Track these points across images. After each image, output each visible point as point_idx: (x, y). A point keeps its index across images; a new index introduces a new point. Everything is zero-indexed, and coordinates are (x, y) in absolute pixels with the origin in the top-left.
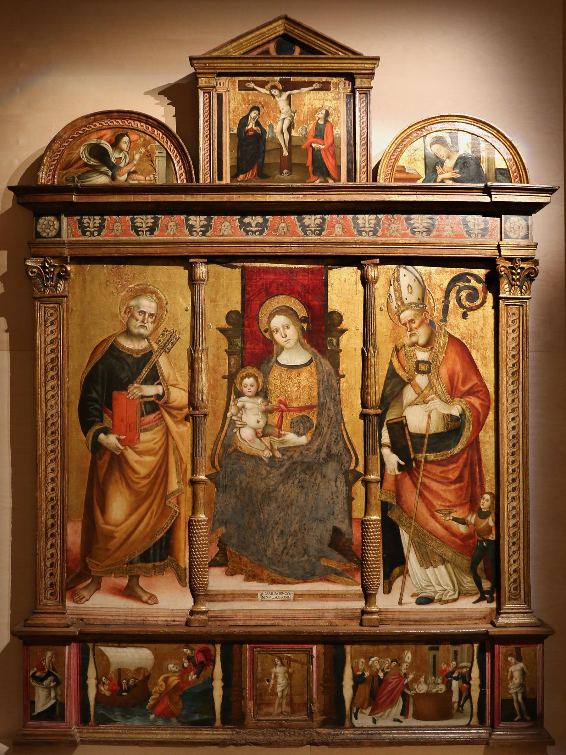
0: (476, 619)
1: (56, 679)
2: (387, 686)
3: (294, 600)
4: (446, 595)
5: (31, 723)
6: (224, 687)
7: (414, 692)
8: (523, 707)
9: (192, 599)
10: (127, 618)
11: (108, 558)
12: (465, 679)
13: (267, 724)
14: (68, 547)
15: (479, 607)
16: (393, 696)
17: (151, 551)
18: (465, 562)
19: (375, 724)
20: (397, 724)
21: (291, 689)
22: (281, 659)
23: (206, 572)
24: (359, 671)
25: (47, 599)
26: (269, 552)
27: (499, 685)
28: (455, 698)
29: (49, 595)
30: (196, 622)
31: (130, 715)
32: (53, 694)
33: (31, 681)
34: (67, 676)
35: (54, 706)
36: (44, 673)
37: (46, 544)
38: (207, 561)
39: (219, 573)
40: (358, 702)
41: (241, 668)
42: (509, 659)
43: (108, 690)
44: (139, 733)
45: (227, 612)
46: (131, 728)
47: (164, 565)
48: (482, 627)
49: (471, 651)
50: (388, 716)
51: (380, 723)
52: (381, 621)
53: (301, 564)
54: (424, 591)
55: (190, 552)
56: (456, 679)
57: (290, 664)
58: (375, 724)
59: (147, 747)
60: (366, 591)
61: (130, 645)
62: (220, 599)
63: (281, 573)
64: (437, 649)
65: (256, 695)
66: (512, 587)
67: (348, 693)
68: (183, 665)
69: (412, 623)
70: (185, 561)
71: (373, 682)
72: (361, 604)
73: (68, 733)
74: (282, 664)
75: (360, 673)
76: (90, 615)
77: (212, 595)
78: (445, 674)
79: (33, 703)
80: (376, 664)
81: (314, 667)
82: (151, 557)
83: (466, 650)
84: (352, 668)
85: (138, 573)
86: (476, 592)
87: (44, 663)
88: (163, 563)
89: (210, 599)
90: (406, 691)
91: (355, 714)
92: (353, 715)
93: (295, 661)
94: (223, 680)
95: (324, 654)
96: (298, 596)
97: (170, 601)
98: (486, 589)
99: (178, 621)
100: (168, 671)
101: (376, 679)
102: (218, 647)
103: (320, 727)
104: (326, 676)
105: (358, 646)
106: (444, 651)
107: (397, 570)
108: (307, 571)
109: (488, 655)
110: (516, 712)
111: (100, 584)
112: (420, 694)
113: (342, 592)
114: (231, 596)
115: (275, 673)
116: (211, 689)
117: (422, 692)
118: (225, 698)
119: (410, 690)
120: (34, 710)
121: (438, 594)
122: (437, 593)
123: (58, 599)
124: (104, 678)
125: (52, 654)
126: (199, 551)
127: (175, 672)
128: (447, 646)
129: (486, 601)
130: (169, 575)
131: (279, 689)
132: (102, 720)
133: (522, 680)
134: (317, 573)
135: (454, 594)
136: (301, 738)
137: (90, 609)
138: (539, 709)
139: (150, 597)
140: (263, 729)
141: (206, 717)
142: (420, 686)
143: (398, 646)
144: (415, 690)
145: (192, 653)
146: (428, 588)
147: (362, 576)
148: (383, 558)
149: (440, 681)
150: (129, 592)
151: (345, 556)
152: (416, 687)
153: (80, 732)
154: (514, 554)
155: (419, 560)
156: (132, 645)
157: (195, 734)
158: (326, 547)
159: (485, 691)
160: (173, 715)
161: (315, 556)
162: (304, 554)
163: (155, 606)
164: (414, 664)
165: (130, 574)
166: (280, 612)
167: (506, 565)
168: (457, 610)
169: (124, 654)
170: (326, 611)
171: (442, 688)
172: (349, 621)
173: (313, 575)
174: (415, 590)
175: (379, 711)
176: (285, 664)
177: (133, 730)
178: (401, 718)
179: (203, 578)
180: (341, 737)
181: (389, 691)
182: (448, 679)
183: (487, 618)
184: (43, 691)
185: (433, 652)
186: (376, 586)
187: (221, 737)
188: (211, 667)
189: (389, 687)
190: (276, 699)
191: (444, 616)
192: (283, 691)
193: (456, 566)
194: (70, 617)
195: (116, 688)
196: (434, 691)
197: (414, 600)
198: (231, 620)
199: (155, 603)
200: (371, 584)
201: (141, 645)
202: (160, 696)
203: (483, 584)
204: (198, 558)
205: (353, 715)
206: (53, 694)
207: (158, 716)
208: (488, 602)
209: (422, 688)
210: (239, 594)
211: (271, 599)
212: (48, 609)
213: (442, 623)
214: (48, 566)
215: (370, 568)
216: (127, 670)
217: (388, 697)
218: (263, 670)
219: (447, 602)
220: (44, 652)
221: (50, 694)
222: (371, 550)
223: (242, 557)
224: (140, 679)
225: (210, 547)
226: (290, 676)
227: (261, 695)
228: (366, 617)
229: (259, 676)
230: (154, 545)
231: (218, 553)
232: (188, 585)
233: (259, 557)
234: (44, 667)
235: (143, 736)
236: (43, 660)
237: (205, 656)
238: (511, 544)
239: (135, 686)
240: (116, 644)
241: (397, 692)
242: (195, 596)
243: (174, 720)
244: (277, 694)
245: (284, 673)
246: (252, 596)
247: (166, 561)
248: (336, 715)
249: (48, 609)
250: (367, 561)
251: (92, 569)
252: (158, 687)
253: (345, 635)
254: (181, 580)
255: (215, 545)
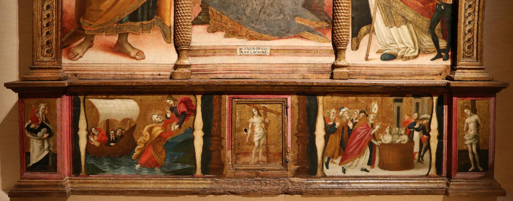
0: (433, 75)
1: (49, 131)
2: (355, 136)
3: (271, 55)
4: (408, 52)
5: (26, 174)
6: (204, 137)
7: (380, 142)
8: (477, 157)
9: (177, 55)
10: (117, 73)
11: (100, 18)
12: (425, 130)
13: (245, 173)
14: (64, 9)
15: (436, 64)
16: (361, 146)
17: (140, 12)
18: (425, 22)
19: (345, 173)
20: (364, 173)
21: (267, 139)
22: (258, 110)
23: (188, 28)
24: (330, 121)
25: (44, 56)
26: (248, 11)
27: (456, 137)
28: (416, 148)
29: (45, 53)
30: (179, 75)
31: (117, 165)
32: (46, 146)
33: (26, 133)
34: (59, 127)
35: (47, 157)
36: (38, 125)
37: (43, 6)
38: (190, 19)
39: (202, 30)
40: (329, 152)
41: (220, 117)
42: (466, 111)
43: (98, 141)
44: (125, 183)
45: (208, 66)
46: (118, 178)
47: (151, 23)
48: (440, 81)
49: (431, 104)
50: (356, 166)
51: (349, 173)
52: (350, 76)
53: (277, 22)
54: (388, 48)
55: (175, 11)
56: (418, 130)
57: (266, 114)
58: (345, 173)
59: (132, 197)
60: (336, 47)
61: (118, 97)
62: (202, 54)
63: (258, 31)
64: (401, 101)
65: (235, 145)
66: (467, 46)
67: (320, 142)
68: (166, 115)
69: (378, 77)
70: (170, 20)
71: (343, 132)
72: (331, 59)
73: (59, 184)
74: (259, 114)
75: (331, 123)
76: (83, 71)
77: (195, 50)
78: (407, 125)
79: (28, 154)
80: (346, 115)
81: (289, 117)
82: (139, 16)
83: (427, 102)
84: (324, 118)
85: (127, 31)
86: (433, 50)
87: (38, 115)
88: (150, 22)
89: (192, 54)
90: (373, 141)
91: (326, 163)
92: (324, 164)
93: (271, 111)
94: (204, 129)
95: (298, 104)
96: (274, 51)
97: (155, 57)
98: (442, 48)
99: (163, 75)
100: (152, 122)
101: (346, 129)
102: (199, 97)
103: (293, 177)
104: (300, 126)
105: (330, 97)
106: (407, 103)
107: (364, 29)
108: (283, 28)
109: (445, 107)
110: (470, 163)
111: (92, 41)
112: (385, 144)
113: (315, 48)
114: (212, 51)
115: (253, 123)
116: (193, 139)
117: (387, 142)
118: (205, 147)
119: (376, 140)
120: (29, 162)
121: (401, 51)
122: (400, 50)
123: (54, 56)
124: (93, 129)
125: (45, 106)
126: (182, 10)
127: (159, 122)
128: (410, 98)
129: (442, 59)
130: (156, 32)
131: (256, 139)
132: (93, 170)
133: (476, 132)
134: (292, 30)
135: (415, 52)
136: (276, 187)
137: (83, 65)
138: (490, 160)
139: (138, 53)
140: (241, 178)
141: (187, 166)
142: (385, 136)
143: (366, 98)
144: (380, 140)
145: (175, 104)
146: (392, 45)
147: (333, 33)
148: (353, 18)
149: (403, 132)
150: (119, 49)
151: (318, 16)
152: (381, 137)
153: (71, 183)
154: (470, 16)
155: (384, 20)
156: (120, 97)
157: (177, 183)
158: (300, 8)
159: (442, 142)
160: (157, 165)
161: (289, 15)
162: (280, 13)
163: (142, 61)
164: (380, 115)
165: (119, 32)
166: (258, 66)
167: (462, 26)
168: (417, 66)
169: (112, 106)
170: (299, 66)
171: (405, 138)
172: (320, 75)
173: (288, 32)
174: (380, 47)
175: (349, 160)
176: (262, 114)
177: (120, 180)
178: (368, 168)
179: (186, 34)
180: (314, 186)
181: (358, 141)
182: (410, 129)
183: (443, 74)
184: (37, 142)
185: (398, 104)
186: (346, 42)
187: (201, 186)
188: (192, 117)
189: (358, 137)
190: (253, 149)
191: (406, 71)
192: (259, 140)
193: (416, 26)
194: (66, 72)
195: (104, 138)
196: (398, 141)
197: (379, 56)
198: (212, 74)
199: (142, 59)
200: (342, 40)
201: (128, 97)
202: (145, 146)
203: (440, 43)
204: (182, 16)
205: (324, 164)
206: (46, 146)
207: (143, 166)
208: (444, 60)
209: (387, 139)
210: (220, 49)
211: (249, 54)
212: (44, 65)
213: (403, 78)
214: (45, 25)
215: (340, 25)
216: (115, 120)
217: (357, 147)
218: (241, 120)
219: (408, 58)
220: (37, 105)
221: (43, 145)
222: (342, 9)
223: (222, 16)
224: (127, 129)
225: (194, 7)
226: (266, 126)
227: (239, 144)
228: (336, 70)
229: (238, 126)
230: (142, 6)
231: (201, 13)
232: (172, 41)
233: (239, 16)
234: (38, 119)
235: (129, 186)
236: (37, 112)
237: (187, 107)
238: (467, 7)
239: (122, 136)
240: (104, 97)
241: (365, 142)
242: (178, 52)
243: (157, 169)
244: (254, 144)
245: (261, 123)
246: (231, 51)
247: (153, 20)
248: (309, 165)
249: (44, 65)
250: (338, 19)
251: (85, 29)
252: (143, 137)
253: (319, 86)
254: (165, 36)
255: (198, 5)
